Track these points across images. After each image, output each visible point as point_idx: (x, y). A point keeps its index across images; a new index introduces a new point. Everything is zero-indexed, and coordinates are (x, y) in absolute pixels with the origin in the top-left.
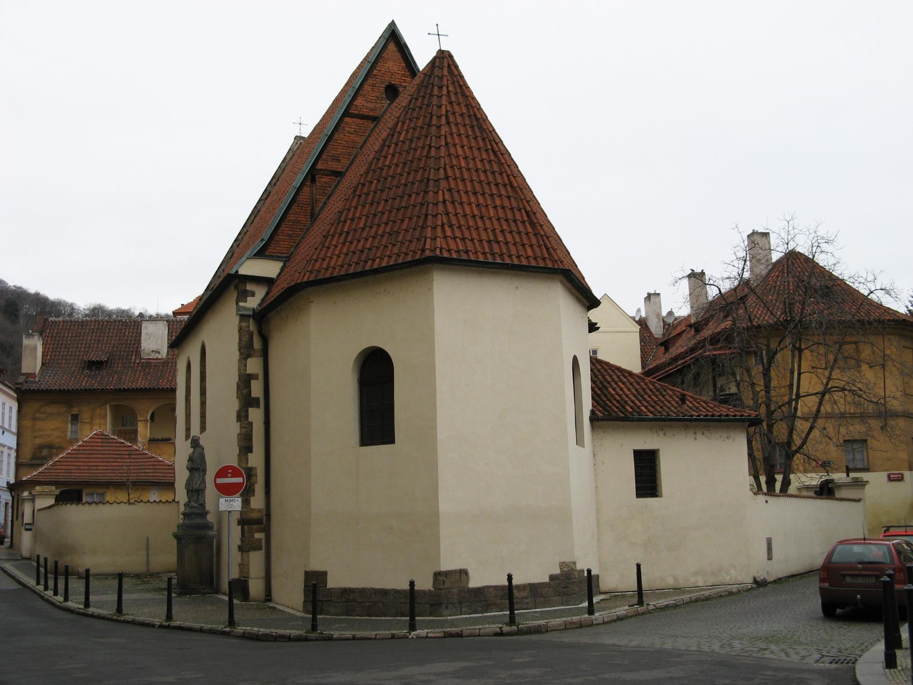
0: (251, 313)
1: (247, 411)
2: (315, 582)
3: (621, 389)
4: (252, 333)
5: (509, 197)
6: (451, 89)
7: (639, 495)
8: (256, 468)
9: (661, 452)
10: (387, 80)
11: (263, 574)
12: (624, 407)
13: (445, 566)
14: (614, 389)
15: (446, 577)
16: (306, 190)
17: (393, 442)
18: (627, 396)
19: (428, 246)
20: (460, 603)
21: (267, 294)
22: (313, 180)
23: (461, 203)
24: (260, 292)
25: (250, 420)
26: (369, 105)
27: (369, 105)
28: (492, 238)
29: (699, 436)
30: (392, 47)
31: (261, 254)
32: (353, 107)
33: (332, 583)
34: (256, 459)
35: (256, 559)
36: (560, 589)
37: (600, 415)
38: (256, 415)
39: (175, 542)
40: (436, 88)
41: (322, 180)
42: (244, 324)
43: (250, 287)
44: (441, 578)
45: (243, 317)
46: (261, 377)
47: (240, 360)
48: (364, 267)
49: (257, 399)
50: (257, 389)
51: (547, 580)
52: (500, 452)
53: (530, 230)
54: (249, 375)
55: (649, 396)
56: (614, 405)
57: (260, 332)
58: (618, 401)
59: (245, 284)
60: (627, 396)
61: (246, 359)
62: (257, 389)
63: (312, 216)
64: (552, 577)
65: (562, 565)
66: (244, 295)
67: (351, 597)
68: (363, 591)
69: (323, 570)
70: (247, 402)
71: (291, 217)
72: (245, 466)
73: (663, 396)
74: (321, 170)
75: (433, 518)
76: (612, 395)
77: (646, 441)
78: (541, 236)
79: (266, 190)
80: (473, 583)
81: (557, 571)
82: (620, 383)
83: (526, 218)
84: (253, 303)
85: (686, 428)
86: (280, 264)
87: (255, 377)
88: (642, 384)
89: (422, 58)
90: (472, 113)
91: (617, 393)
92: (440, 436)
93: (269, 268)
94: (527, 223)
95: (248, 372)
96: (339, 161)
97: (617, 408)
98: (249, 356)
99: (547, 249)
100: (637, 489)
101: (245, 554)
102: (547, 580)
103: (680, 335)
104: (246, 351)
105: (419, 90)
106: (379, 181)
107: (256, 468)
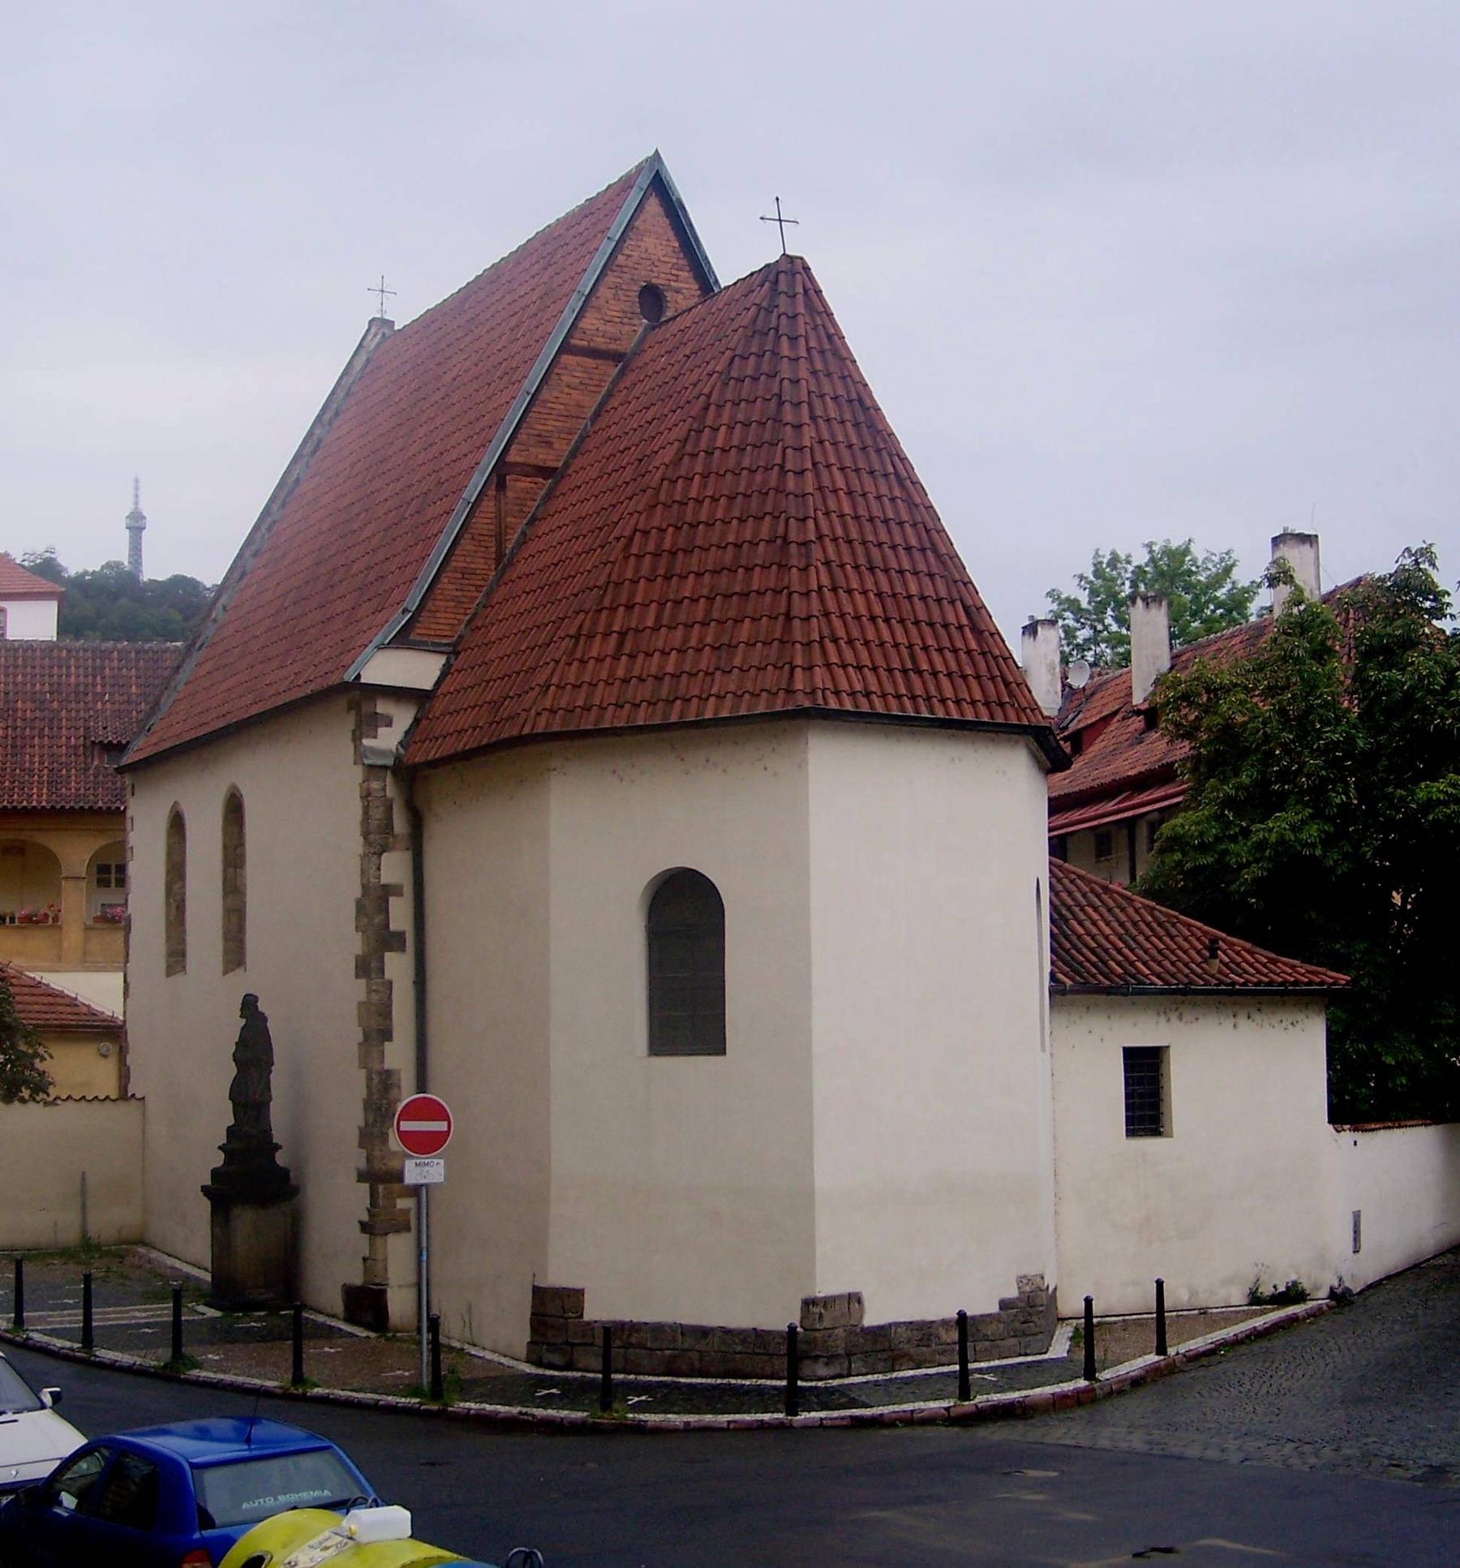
0: (390, 762)
1: (382, 960)
2: (554, 1312)
3: (1094, 923)
4: (391, 801)
5: (931, 575)
6: (812, 344)
7: (1131, 1132)
8: (398, 1071)
9: (1172, 1053)
10: (643, 276)
11: (413, 1279)
12: (1105, 963)
13: (823, 1290)
14: (1081, 923)
15: (825, 1306)
16: (488, 506)
17: (722, 1051)
18: (1106, 937)
19: (799, 686)
20: (849, 1355)
21: (417, 721)
22: (501, 486)
23: (849, 592)
24: (403, 718)
25: (387, 976)
26: (609, 328)
27: (609, 328)
28: (909, 665)
29: (1242, 1021)
30: (654, 205)
31: (403, 640)
32: (578, 334)
33: (595, 1311)
34: (398, 1054)
35: (398, 1250)
36: (1017, 1325)
37: (1069, 982)
38: (399, 967)
39: (206, 1204)
40: (784, 339)
41: (518, 485)
42: (375, 785)
43: (383, 707)
44: (816, 1310)
45: (372, 770)
46: (408, 890)
47: (363, 857)
48: (666, 715)
49: (401, 935)
50: (400, 915)
51: (994, 1309)
52: (924, 1083)
53: (973, 645)
54: (385, 886)
55: (1147, 939)
56: (1088, 960)
57: (415, 791)
58: (1093, 951)
59: (373, 700)
60: (1106, 937)
61: (380, 855)
62: (400, 915)
63: (499, 558)
64: (1004, 1305)
65: (1021, 1280)
66: (369, 723)
67: (633, 1340)
68: (658, 1329)
69: (578, 1285)
70: (386, 940)
71: (457, 562)
72: (377, 1067)
73: (1172, 938)
74: (517, 464)
75: (803, 1200)
76: (1079, 937)
77: (1145, 1031)
78: (995, 658)
79: (310, 434)
80: (872, 1317)
81: (1012, 1293)
82: (1089, 910)
83: (965, 621)
84: (388, 739)
85: (1219, 1007)
86: (442, 660)
87: (397, 890)
88: (1131, 911)
89: (733, 257)
90: (854, 396)
91: (1089, 934)
92: (816, 1048)
93: (419, 670)
94: (967, 630)
95: (383, 881)
96: (549, 444)
97: (1094, 965)
98: (384, 849)
99: (1007, 684)
100: (1129, 1120)
101: (379, 1241)
102: (994, 1309)
103: (1106, 720)
104: (377, 838)
105: (748, 340)
106: (678, 528)
107: (398, 1071)
